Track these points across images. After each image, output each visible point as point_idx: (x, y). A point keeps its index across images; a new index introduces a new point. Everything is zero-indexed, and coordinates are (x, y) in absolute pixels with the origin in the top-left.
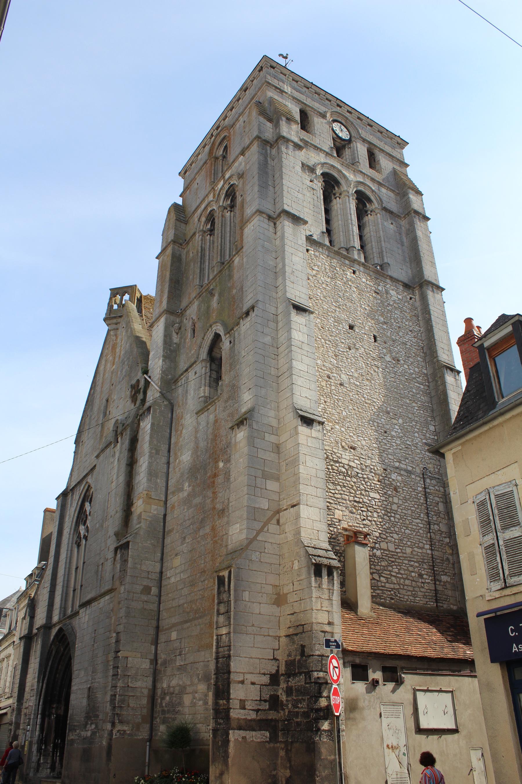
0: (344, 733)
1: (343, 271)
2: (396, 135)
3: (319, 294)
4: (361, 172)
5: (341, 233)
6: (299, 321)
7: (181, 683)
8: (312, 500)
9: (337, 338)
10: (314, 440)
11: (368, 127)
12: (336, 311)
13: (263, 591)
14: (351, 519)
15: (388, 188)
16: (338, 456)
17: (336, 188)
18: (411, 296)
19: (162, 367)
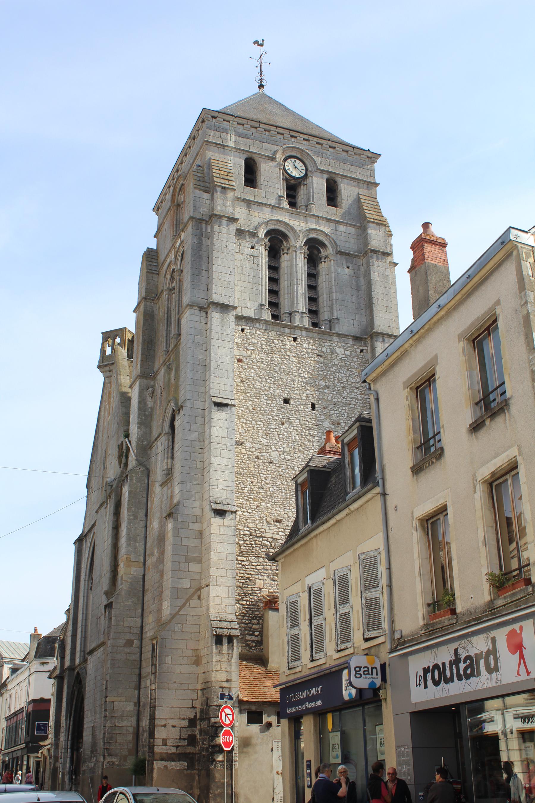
0: (237, 763)
1: (282, 341)
2: (364, 150)
3: (252, 375)
5: (286, 295)
8: (221, 580)
9: (268, 416)
10: (226, 528)
11: (330, 150)
13: (184, 654)
14: (272, 587)
15: (347, 224)
16: (261, 532)
17: (284, 243)
18: (361, 348)
19: (138, 434)
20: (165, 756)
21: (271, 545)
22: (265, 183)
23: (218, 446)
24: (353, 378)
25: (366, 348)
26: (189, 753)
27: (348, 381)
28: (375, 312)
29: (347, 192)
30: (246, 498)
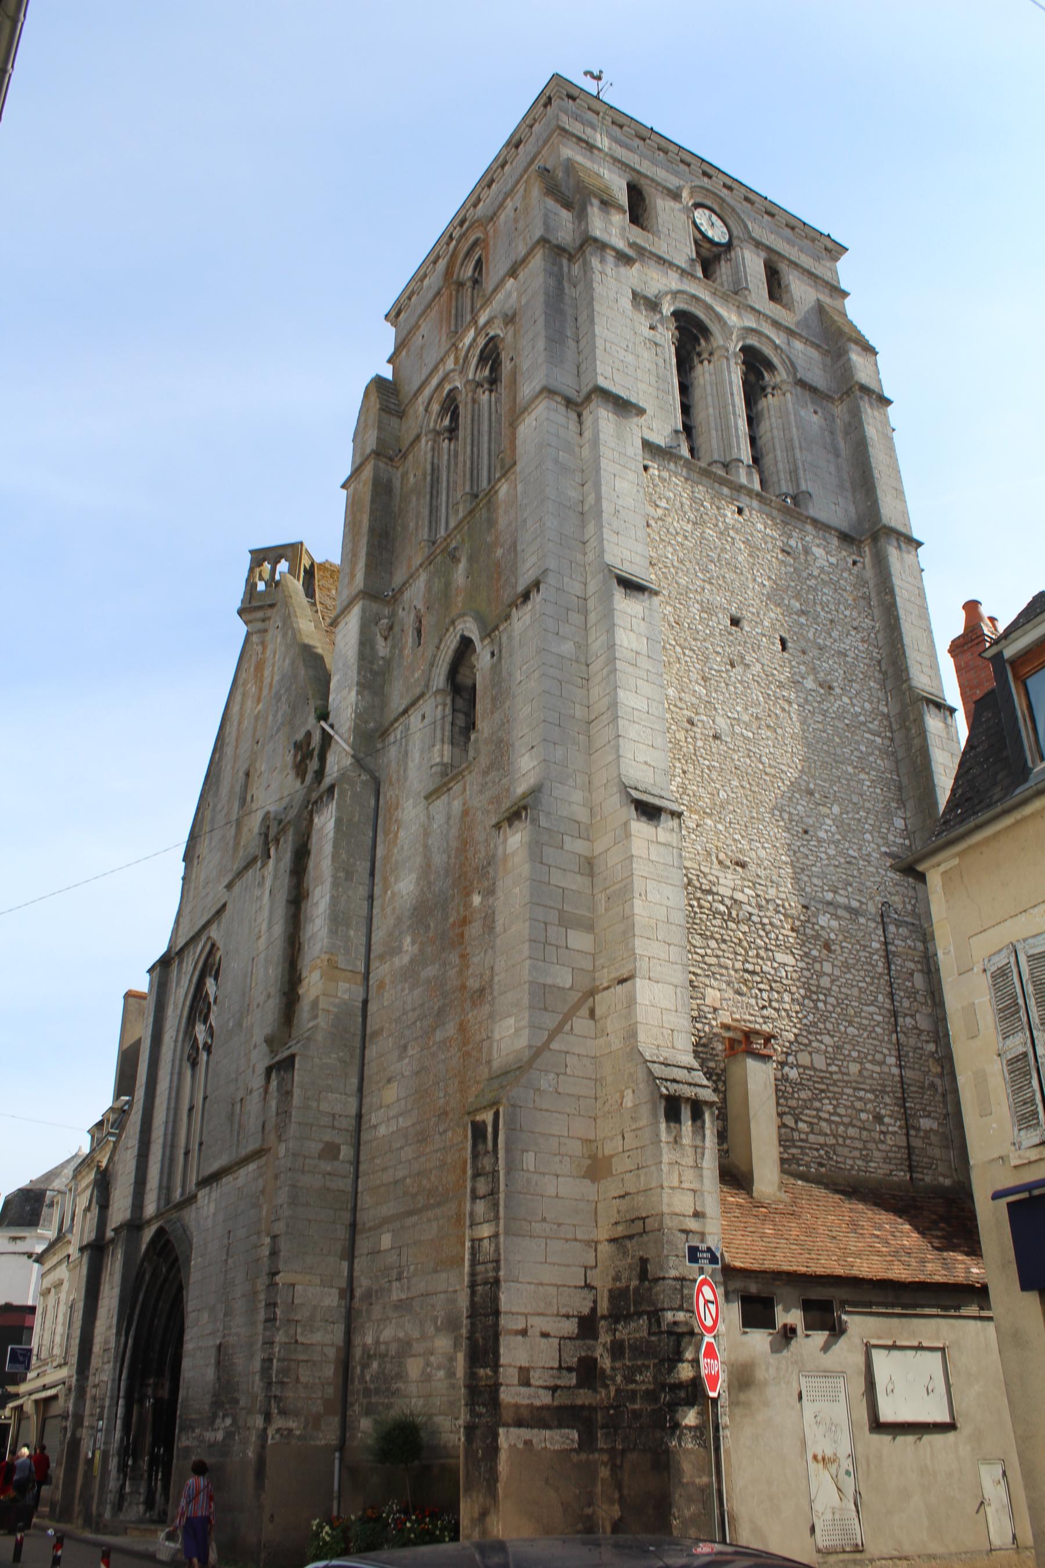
0: (727, 1432)
1: (718, 508)
3: (670, 556)
5: (714, 433)
6: (629, 611)
7: (401, 1335)
11: (766, 217)
14: (737, 1007)
15: (807, 340)
16: (710, 881)
17: (702, 341)
18: (854, 557)
20: (525, 1413)
21: (730, 913)
23: (630, 669)
26: (582, 1407)
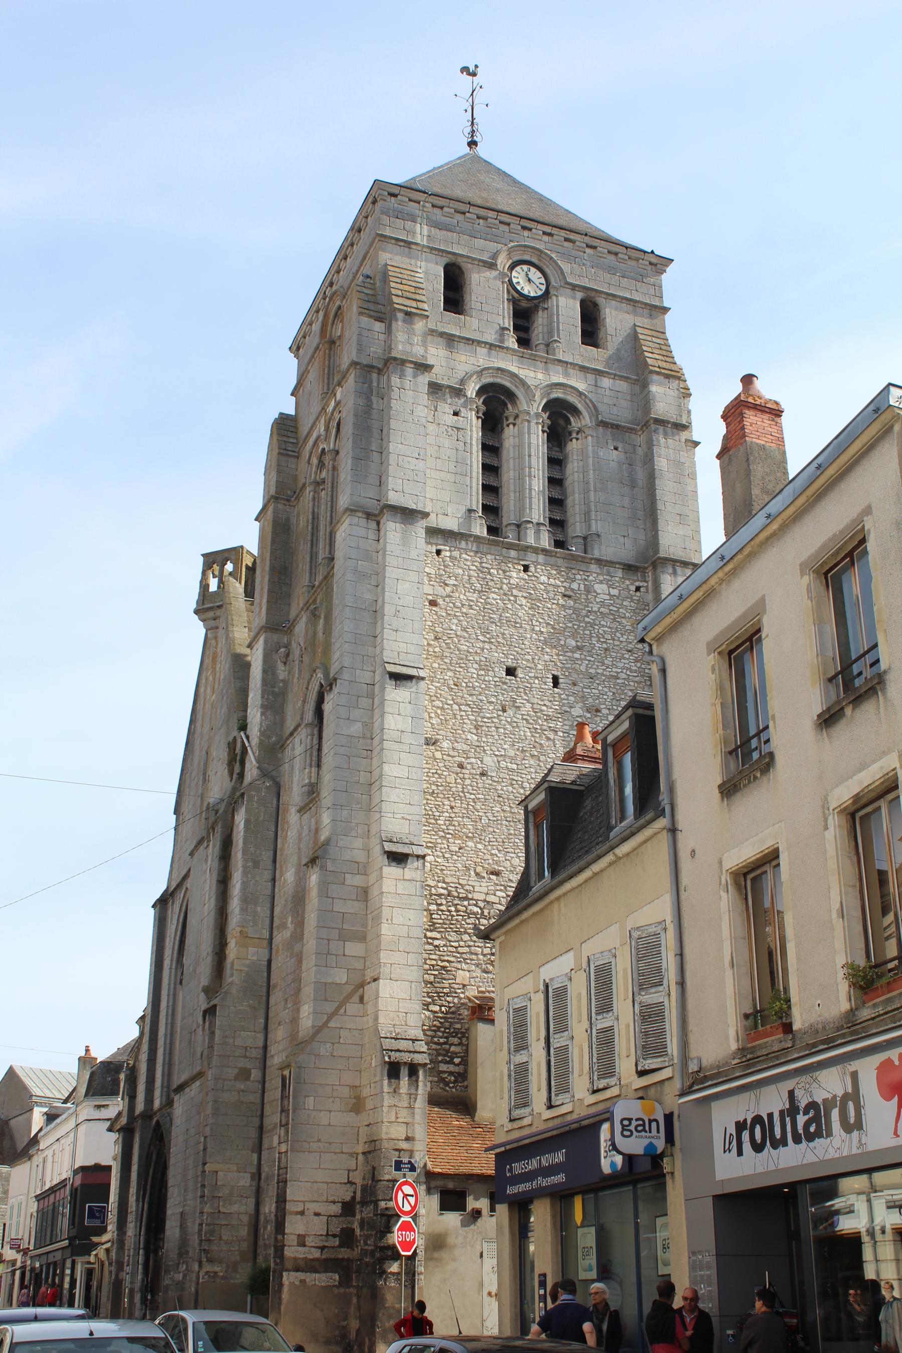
0: (422, 1277)
1: (504, 572)
2: (645, 252)
3: (454, 628)
4: (560, 361)
5: (512, 494)
6: (398, 699)
9: (480, 697)
10: (408, 883)
11: (588, 251)
12: (483, 649)
14: (483, 982)
15: (615, 375)
17: (509, 406)
18: (637, 584)
20: (301, 1263)
21: (482, 912)
22: (478, 306)
23: (395, 746)
24: (622, 635)
25: (645, 584)
26: (343, 1259)
27: (614, 640)
28: (661, 524)
29: (615, 322)
30: (441, 834)
